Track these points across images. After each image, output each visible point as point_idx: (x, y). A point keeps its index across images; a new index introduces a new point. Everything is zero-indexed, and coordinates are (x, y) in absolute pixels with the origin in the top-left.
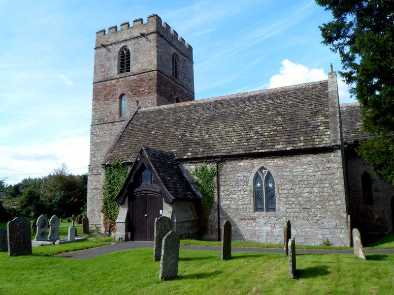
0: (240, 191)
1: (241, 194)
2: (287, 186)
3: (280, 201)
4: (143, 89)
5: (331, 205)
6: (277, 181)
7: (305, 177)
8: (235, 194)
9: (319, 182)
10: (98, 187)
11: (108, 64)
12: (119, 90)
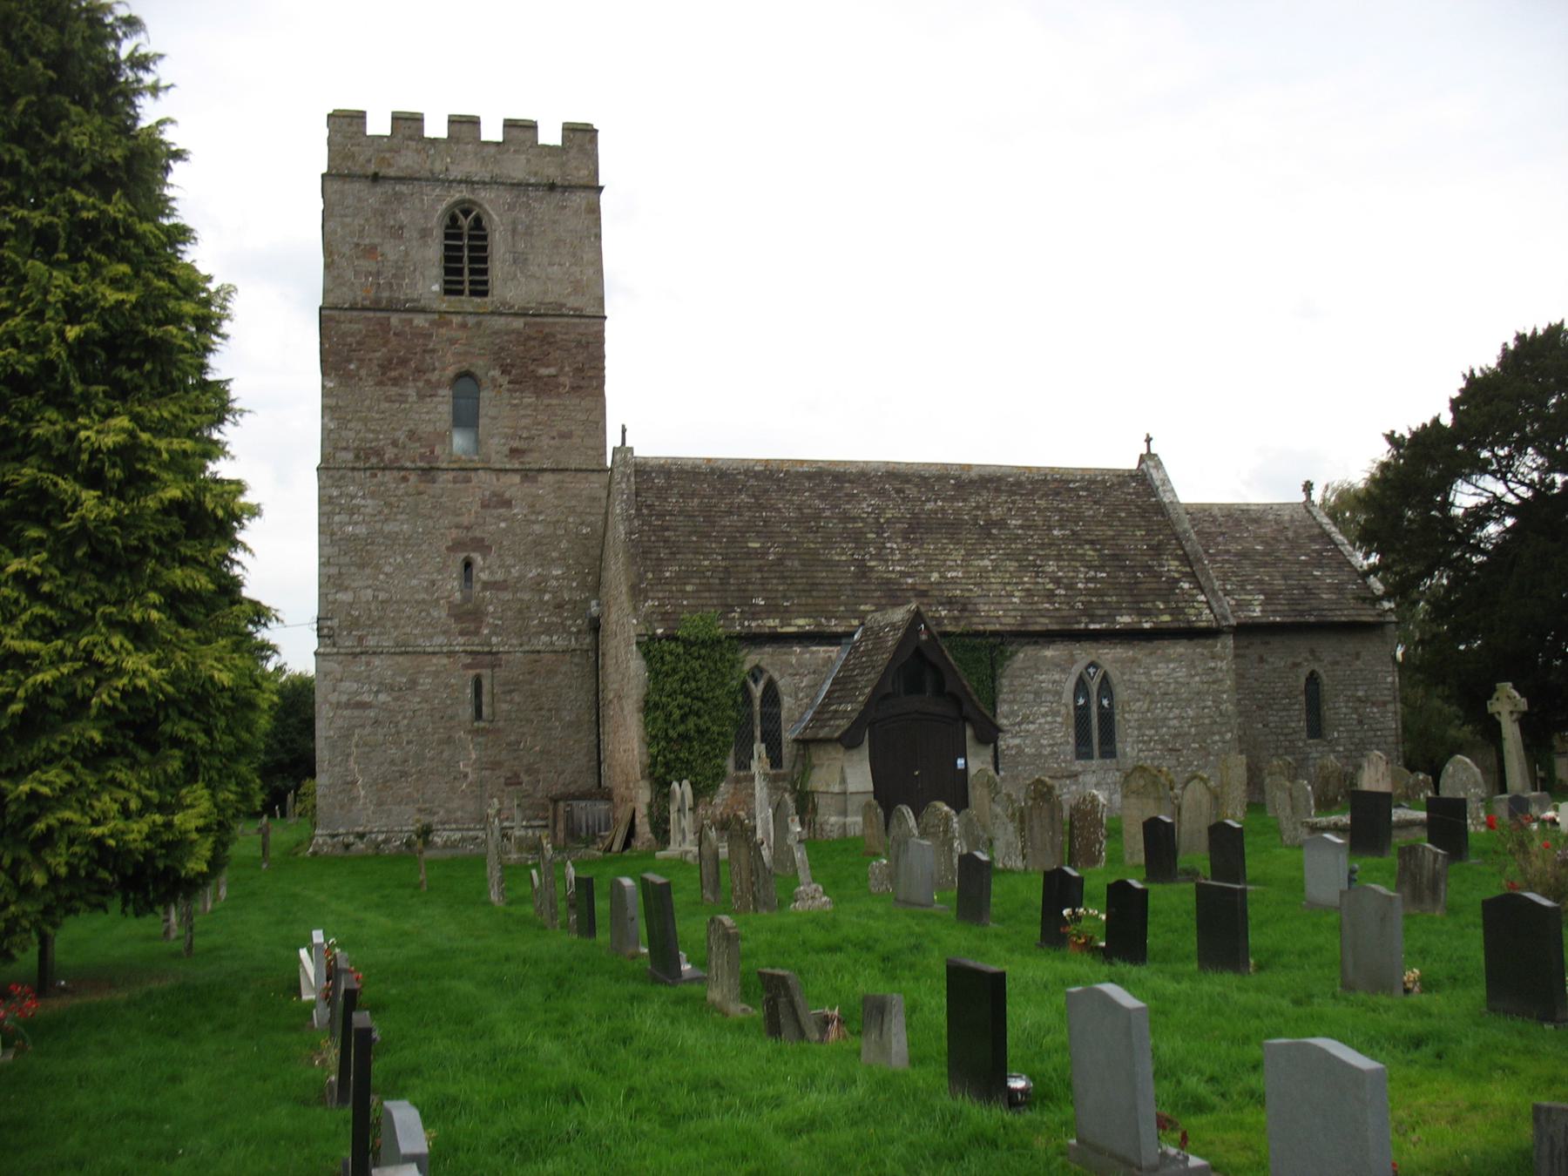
0: (1045, 715)
1: (1046, 723)
2: (1138, 704)
3: (1127, 735)
4: (552, 371)
5: (1215, 742)
6: (1121, 693)
7: (1172, 686)
8: (1032, 723)
9: (1197, 697)
10: (366, 698)
11: (392, 251)
12: (449, 358)
